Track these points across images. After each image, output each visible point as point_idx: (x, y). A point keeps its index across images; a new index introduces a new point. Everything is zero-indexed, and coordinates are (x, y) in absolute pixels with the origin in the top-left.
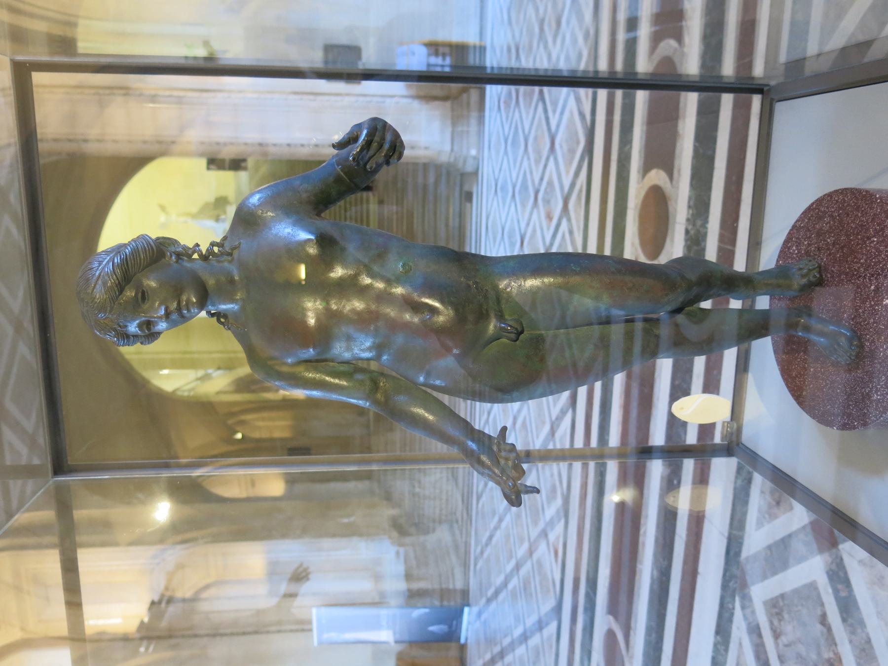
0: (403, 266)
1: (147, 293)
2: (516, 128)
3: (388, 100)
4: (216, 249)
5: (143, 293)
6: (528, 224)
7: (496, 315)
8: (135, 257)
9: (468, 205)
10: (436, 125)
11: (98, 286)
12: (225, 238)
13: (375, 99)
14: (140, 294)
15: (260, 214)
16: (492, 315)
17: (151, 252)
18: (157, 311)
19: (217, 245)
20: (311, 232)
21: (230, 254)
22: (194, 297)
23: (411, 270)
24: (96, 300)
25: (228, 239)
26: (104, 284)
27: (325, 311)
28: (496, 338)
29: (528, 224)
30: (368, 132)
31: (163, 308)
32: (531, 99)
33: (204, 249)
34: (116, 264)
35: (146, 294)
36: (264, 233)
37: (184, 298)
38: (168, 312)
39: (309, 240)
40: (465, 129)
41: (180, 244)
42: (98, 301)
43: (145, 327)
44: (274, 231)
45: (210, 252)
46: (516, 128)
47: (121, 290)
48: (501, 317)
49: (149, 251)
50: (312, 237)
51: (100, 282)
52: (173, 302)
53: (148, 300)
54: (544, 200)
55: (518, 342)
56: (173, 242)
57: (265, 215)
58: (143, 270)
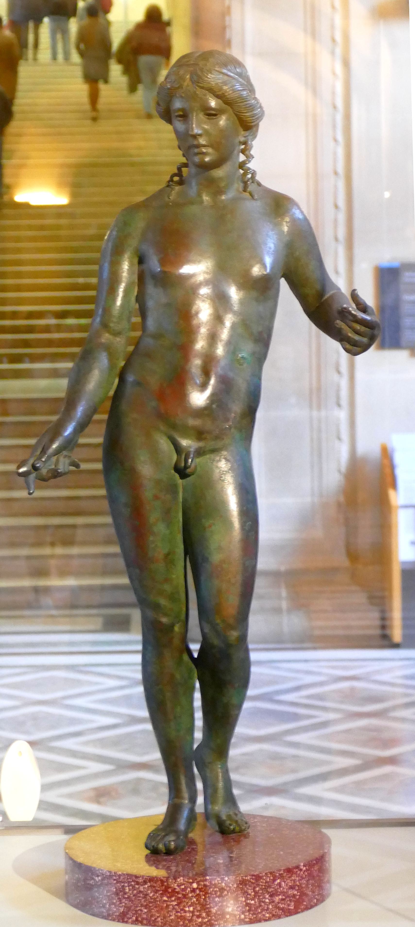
0: (243, 357)
1: (215, 119)
2: (296, 717)
3: (342, 415)
4: (249, 176)
5: (215, 115)
6: (74, 754)
7: (200, 448)
8: (247, 109)
9: (99, 622)
10: (78, 861)
11: (221, 76)
12: (259, 184)
13: (344, 383)
14: (214, 112)
15: (285, 220)
16: (201, 444)
17: (252, 121)
18: (199, 126)
19: (253, 177)
20: (272, 268)
21: (245, 190)
22: (210, 160)
23: (240, 365)
24: (210, 75)
25: (259, 188)
26: (225, 83)
27: (198, 282)
28: (178, 448)
29: (74, 754)
30: (369, 320)
31: (200, 132)
32: (365, 744)
33: (251, 165)
34: (242, 93)
35: (214, 117)
36: (269, 223)
37: (210, 150)
38: (197, 137)
39: (265, 267)
40: (284, 605)
41: (252, 141)
42: (209, 77)
43: (181, 113)
44: (271, 233)
45: (247, 171)
46: (296, 717)
47: (218, 97)
48: (200, 453)
49: (253, 120)
50: (268, 270)
51: (226, 78)
52: (206, 141)
53: (208, 119)
54: (139, 780)
55: (173, 471)
56: (255, 137)
57: (284, 223)
58: (236, 115)
